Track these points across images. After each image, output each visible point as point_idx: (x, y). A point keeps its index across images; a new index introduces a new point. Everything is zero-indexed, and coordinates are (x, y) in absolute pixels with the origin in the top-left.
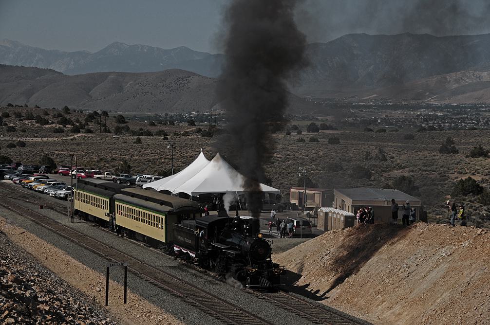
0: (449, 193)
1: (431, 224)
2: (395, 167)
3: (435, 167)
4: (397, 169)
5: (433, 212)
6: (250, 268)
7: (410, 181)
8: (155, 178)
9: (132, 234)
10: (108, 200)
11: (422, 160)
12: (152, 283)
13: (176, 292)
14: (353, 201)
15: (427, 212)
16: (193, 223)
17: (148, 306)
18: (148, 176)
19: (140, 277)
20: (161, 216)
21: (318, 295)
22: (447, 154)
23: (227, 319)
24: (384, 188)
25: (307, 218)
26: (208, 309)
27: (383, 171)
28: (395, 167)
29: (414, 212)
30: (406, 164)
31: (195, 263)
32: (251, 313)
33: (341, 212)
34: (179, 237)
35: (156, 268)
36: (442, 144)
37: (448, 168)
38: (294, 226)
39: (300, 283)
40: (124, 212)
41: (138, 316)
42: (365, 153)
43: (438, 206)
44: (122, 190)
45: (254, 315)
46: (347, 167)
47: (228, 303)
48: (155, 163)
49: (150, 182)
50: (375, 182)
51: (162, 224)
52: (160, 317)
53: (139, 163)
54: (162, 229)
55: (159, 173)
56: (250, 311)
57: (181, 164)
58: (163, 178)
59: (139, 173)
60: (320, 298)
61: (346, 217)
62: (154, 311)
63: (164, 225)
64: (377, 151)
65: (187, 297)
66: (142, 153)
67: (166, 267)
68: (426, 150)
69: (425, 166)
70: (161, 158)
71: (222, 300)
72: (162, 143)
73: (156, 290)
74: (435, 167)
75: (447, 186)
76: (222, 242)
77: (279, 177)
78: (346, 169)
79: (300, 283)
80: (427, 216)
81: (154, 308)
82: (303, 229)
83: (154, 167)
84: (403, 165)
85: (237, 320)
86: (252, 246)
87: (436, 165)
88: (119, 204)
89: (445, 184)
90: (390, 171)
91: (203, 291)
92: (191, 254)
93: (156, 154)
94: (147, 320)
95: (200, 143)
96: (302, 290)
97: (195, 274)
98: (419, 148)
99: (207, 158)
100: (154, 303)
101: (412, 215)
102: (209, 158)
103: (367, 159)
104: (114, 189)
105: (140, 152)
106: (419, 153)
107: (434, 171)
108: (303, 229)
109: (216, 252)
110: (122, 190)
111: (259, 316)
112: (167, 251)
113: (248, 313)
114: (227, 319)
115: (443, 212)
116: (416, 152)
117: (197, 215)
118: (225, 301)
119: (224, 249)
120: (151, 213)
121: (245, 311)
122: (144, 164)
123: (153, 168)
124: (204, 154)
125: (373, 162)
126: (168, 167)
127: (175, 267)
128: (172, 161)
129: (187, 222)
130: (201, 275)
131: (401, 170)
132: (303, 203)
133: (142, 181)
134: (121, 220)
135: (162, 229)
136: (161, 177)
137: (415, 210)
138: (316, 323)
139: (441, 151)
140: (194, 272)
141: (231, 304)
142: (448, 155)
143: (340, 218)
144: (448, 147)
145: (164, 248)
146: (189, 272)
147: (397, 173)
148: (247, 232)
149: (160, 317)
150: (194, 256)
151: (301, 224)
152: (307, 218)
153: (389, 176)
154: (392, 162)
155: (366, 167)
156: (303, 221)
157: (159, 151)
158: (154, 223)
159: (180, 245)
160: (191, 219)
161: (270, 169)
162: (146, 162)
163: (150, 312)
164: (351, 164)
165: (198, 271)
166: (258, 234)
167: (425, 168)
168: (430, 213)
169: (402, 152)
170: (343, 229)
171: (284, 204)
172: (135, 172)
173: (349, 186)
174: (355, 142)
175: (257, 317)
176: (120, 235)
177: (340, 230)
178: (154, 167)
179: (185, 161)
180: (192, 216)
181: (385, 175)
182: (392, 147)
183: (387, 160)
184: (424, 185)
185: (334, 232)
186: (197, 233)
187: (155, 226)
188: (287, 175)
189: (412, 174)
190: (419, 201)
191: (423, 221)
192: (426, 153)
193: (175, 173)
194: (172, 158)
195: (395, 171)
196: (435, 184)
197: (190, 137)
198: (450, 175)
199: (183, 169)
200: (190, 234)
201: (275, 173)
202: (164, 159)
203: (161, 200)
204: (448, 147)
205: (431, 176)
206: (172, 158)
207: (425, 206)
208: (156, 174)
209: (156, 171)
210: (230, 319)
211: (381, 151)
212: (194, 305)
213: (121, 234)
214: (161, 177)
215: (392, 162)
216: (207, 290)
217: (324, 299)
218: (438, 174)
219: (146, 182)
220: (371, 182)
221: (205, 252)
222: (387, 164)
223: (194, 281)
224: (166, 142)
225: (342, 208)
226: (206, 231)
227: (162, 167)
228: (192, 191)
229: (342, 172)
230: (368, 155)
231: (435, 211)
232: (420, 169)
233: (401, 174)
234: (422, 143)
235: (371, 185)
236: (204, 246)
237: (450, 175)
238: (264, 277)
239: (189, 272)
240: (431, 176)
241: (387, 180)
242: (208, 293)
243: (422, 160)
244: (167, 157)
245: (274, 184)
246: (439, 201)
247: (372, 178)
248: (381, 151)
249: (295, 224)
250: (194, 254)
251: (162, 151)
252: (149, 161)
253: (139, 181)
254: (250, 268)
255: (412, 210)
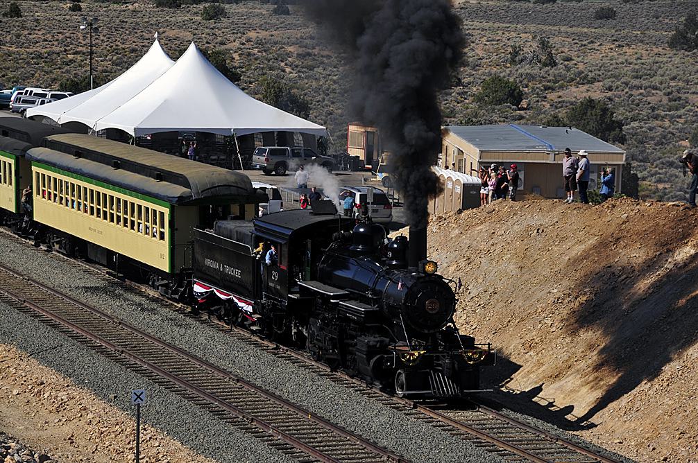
0: (688, 136)
1: (644, 201)
2: (572, 80)
3: (658, 78)
4: (578, 83)
5: (652, 176)
6: (407, 349)
7: (605, 110)
8: (53, 96)
9: (78, 248)
10: (12, 161)
11: (630, 64)
12: (47, 322)
13: (98, 342)
14: (481, 152)
15: (639, 176)
16: (247, 227)
17: (37, 370)
18: (36, 90)
19: (20, 309)
20: (159, 208)
21: (569, 417)
22: (686, 50)
23: (233, 414)
24: (549, 124)
25: (383, 188)
26: (167, 378)
27: (547, 88)
28: (572, 80)
29: (610, 175)
30: (597, 72)
31: (254, 328)
32: (260, 388)
33: (456, 175)
34: (208, 262)
35: (55, 291)
36: (677, 28)
37: (687, 82)
38: (356, 205)
39: (519, 384)
40: (58, 193)
41: (15, 393)
42: (510, 50)
43: (662, 163)
44: (50, 138)
45: (266, 392)
46: (471, 79)
47: (211, 366)
48: (53, 62)
49: (43, 103)
50: (528, 112)
51: (163, 226)
52: (63, 395)
53: (16, 60)
54: (162, 237)
55: (61, 85)
56: (259, 383)
57: (110, 67)
58: (70, 95)
59: (17, 82)
60: (578, 425)
61: (467, 188)
62: (49, 381)
63: (166, 230)
64: (535, 45)
65: (122, 352)
66: (23, 39)
67: (78, 287)
68: (642, 41)
69: (637, 77)
70: (65, 51)
71: (199, 360)
72: (68, 17)
73: (56, 338)
74: (658, 78)
75: (682, 121)
76: (327, 279)
77: (324, 99)
78: (469, 83)
79: (519, 384)
80: (638, 185)
81: (51, 376)
82: (374, 211)
83: (51, 72)
84: (591, 75)
85: (314, 447)
86: (411, 294)
87: (662, 76)
88: (42, 171)
89: (680, 117)
90: (562, 87)
91: (159, 340)
92: (241, 304)
93: (56, 43)
94: (34, 400)
95: (153, 21)
96: (526, 403)
97: (140, 304)
98: (625, 37)
99: (168, 55)
100: (50, 364)
101: (604, 182)
102: (175, 53)
103: (513, 62)
104: (26, 133)
105: (18, 36)
106: (625, 49)
107: (656, 89)
108: (374, 211)
109: (309, 306)
110: (50, 138)
111: (277, 393)
112: (175, 292)
113: (254, 386)
114: (208, 400)
115: (671, 176)
116: (620, 46)
117: (249, 208)
118: (207, 363)
119: (334, 297)
120: (59, 176)
121: (248, 383)
122: (28, 63)
123: (47, 73)
124: (161, 45)
125: (525, 69)
126: (82, 72)
127: (97, 289)
128: (91, 59)
129: (230, 225)
130: (154, 306)
131: (586, 87)
132: (375, 158)
133: (24, 102)
134: (46, 212)
135: (162, 237)
136: (66, 94)
137: (613, 172)
138: (397, 408)
139: (673, 44)
140: (137, 299)
141: (218, 369)
142: (687, 53)
143: (454, 188)
144: (689, 35)
145: (162, 285)
146: (128, 300)
147: (578, 93)
148: (392, 259)
149: (63, 395)
150: (250, 309)
151: (370, 200)
152: (383, 188)
153: (560, 100)
154: (568, 69)
155: (511, 80)
156: (375, 195)
157: (61, 36)
158: (50, 193)
159: (208, 277)
160: (236, 218)
161: (306, 81)
162: (32, 58)
163: (42, 383)
164: (480, 72)
165: (147, 297)
166: (424, 265)
167: (637, 82)
168: (644, 179)
169: (590, 46)
170: (460, 212)
171: (335, 156)
172: (9, 80)
173: (474, 120)
174: (490, 24)
175: (273, 395)
176: (43, 247)
177: (452, 213)
178: (51, 72)
179: (121, 58)
180: (235, 209)
181: (552, 96)
182: (568, 35)
183: (555, 64)
184: (633, 120)
185: (440, 218)
186: (258, 252)
187: (46, 196)
188: (343, 96)
189: (610, 94)
190: (623, 154)
191: (629, 195)
192: (641, 49)
193: (97, 85)
194: (91, 53)
195: (574, 89)
196: (656, 117)
197: (130, 7)
198: (690, 97)
199: (115, 77)
200: (238, 256)
201: (317, 90)
202: (74, 54)
203: (155, 169)
204: (689, 35)
205: (649, 99)
206: (91, 53)
207: (635, 164)
208: (56, 86)
209: (54, 80)
210: (216, 400)
211: (544, 45)
212: (137, 370)
213: (44, 243)
214: (66, 94)
215: (568, 69)
216: (167, 339)
217: (583, 428)
218: (665, 94)
219: (33, 102)
220: (522, 112)
221: (281, 302)
222: (557, 72)
223: (140, 319)
224: (77, 17)
225: (459, 167)
226: (285, 249)
227: (68, 72)
228: (136, 126)
229: (459, 89)
230: (517, 53)
231: (656, 173)
232: (627, 84)
233: (584, 94)
234: (633, 27)
235: (521, 118)
236: (278, 287)
237: (690, 97)
238: (441, 371)
239: (128, 300)
240: (649, 99)
241: (556, 108)
242: (169, 345)
243: (630, 64)
244: (80, 49)
245: (313, 114)
246: (664, 154)
247: (524, 103)
248: (544, 45)
249: (358, 202)
250: (249, 304)
251: (68, 35)
252: (40, 56)
253: (17, 100)
254: (407, 349)
255: (605, 172)
